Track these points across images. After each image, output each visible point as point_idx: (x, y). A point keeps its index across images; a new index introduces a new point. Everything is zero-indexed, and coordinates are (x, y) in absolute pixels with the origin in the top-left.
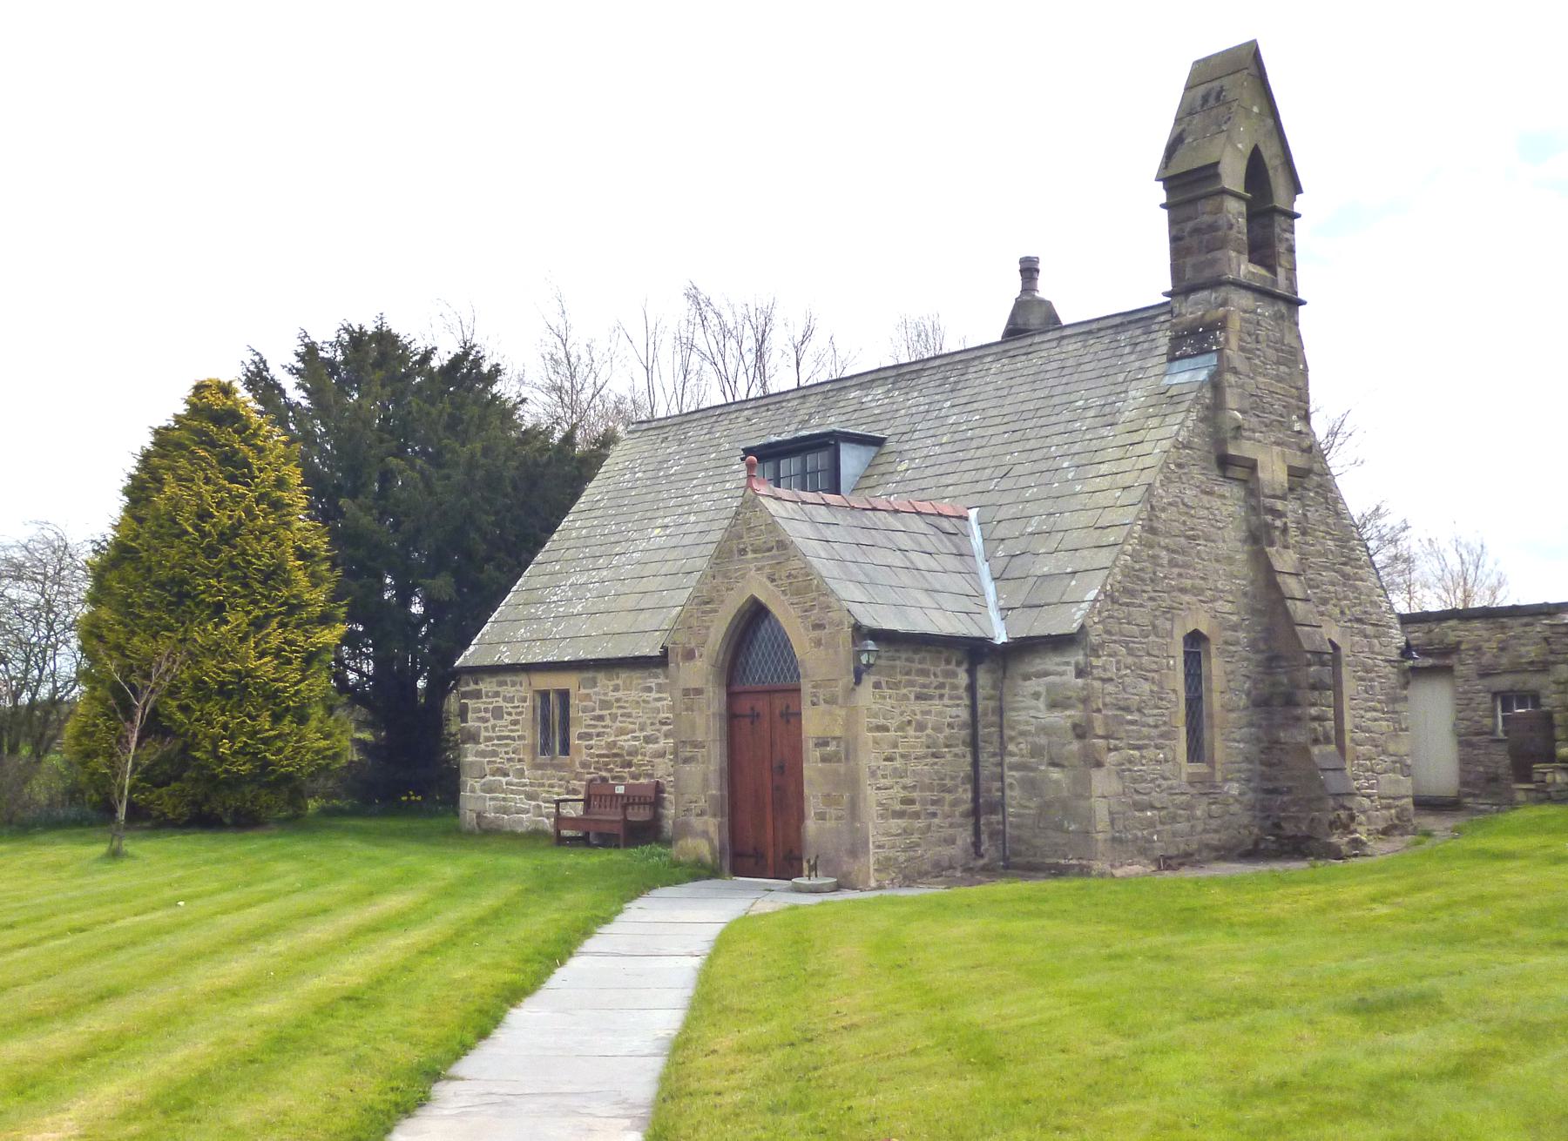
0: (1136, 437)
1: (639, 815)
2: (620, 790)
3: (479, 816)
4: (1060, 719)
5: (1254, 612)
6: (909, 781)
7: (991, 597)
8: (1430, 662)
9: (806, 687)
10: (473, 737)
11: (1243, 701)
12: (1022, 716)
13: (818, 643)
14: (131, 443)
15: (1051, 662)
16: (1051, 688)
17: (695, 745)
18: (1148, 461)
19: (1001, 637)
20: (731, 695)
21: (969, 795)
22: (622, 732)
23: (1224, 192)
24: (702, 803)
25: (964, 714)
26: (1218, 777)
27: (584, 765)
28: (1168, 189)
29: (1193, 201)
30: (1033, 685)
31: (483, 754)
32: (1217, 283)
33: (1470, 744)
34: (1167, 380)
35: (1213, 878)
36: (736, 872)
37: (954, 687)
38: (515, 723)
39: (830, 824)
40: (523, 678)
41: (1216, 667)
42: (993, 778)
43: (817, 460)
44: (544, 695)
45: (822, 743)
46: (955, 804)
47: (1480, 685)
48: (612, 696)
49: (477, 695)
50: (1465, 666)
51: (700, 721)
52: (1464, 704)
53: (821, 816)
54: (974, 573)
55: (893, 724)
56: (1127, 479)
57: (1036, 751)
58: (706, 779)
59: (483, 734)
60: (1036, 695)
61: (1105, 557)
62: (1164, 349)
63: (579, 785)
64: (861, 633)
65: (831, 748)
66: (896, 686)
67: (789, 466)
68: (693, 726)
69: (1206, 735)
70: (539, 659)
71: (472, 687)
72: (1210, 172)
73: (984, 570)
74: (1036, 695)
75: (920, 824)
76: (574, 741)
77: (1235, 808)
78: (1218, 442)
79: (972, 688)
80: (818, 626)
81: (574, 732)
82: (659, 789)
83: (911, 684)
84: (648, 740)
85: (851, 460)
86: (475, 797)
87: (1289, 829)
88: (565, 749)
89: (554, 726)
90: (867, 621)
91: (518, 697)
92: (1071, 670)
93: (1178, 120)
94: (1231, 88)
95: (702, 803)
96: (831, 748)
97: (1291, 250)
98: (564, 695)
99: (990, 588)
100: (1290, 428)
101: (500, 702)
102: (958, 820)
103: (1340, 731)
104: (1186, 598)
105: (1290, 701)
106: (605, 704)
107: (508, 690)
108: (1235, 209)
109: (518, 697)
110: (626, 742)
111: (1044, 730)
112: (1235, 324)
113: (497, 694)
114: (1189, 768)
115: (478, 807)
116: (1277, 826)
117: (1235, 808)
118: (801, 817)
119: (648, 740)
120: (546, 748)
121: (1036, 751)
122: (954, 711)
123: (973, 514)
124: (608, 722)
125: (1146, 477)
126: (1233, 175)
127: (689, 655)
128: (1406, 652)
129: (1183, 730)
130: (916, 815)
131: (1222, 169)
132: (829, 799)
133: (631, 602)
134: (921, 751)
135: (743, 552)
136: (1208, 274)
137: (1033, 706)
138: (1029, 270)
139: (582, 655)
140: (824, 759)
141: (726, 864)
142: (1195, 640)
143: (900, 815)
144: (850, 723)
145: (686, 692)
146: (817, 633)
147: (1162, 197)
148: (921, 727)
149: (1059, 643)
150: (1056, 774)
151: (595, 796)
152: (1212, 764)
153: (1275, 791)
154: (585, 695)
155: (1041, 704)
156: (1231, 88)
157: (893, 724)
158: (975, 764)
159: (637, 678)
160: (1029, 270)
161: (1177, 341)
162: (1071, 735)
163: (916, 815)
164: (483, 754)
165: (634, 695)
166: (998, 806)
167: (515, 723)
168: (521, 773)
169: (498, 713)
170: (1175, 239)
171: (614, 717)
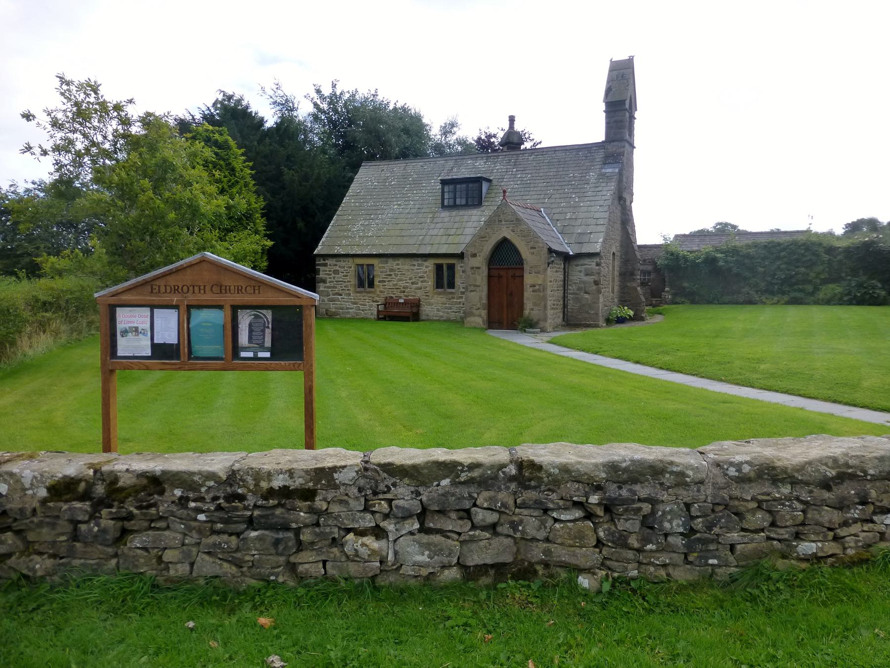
2: (401, 301)
9: (526, 267)
10: (324, 281)
12: (575, 278)
13: (533, 253)
14: (860, 218)
16: (586, 270)
17: (475, 286)
18: (606, 198)
20: (489, 269)
22: (401, 280)
27: (381, 292)
28: (607, 106)
29: (616, 111)
30: (579, 268)
34: (603, 171)
39: (534, 312)
40: (351, 260)
44: (362, 265)
48: (396, 267)
49: (325, 265)
51: (479, 278)
56: (601, 203)
57: (579, 289)
58: (481, 298)
59: (328, 280)
64: (550, 251)
65: (537, 287)
71: (322, 262)
74: (580, 271)
76: (376, 283)
79: (564, 269)
80: (532, 248)
84: (413, 283)
90: (555, 247)
91: (350, 266)
92: (594, 264)
93: (608, 82)
95: (478, 306)
96: (537, 287)
101: (337, 268)
106: (392, 270)
107: (342, 264)
113: (336, 265)
115: (327, 307)
119: (413, 283)
121: (579, 289)
124: (393, 276)
127: (474, 255)
132: (535, 304)
137: (578, 274)
138: (512, 120)
140: (533, 291)
144: (544, 280)
145: (472, 268)
146: (532, 250)
150: (587, 296)
154: (380, 269)
155: (582, 274)
159: (408, 261)
160: (512, 120)
161: (607, 157)
162: (593, 284)
165: (406, 267)
170: (608, 123)
171: (396, 275)
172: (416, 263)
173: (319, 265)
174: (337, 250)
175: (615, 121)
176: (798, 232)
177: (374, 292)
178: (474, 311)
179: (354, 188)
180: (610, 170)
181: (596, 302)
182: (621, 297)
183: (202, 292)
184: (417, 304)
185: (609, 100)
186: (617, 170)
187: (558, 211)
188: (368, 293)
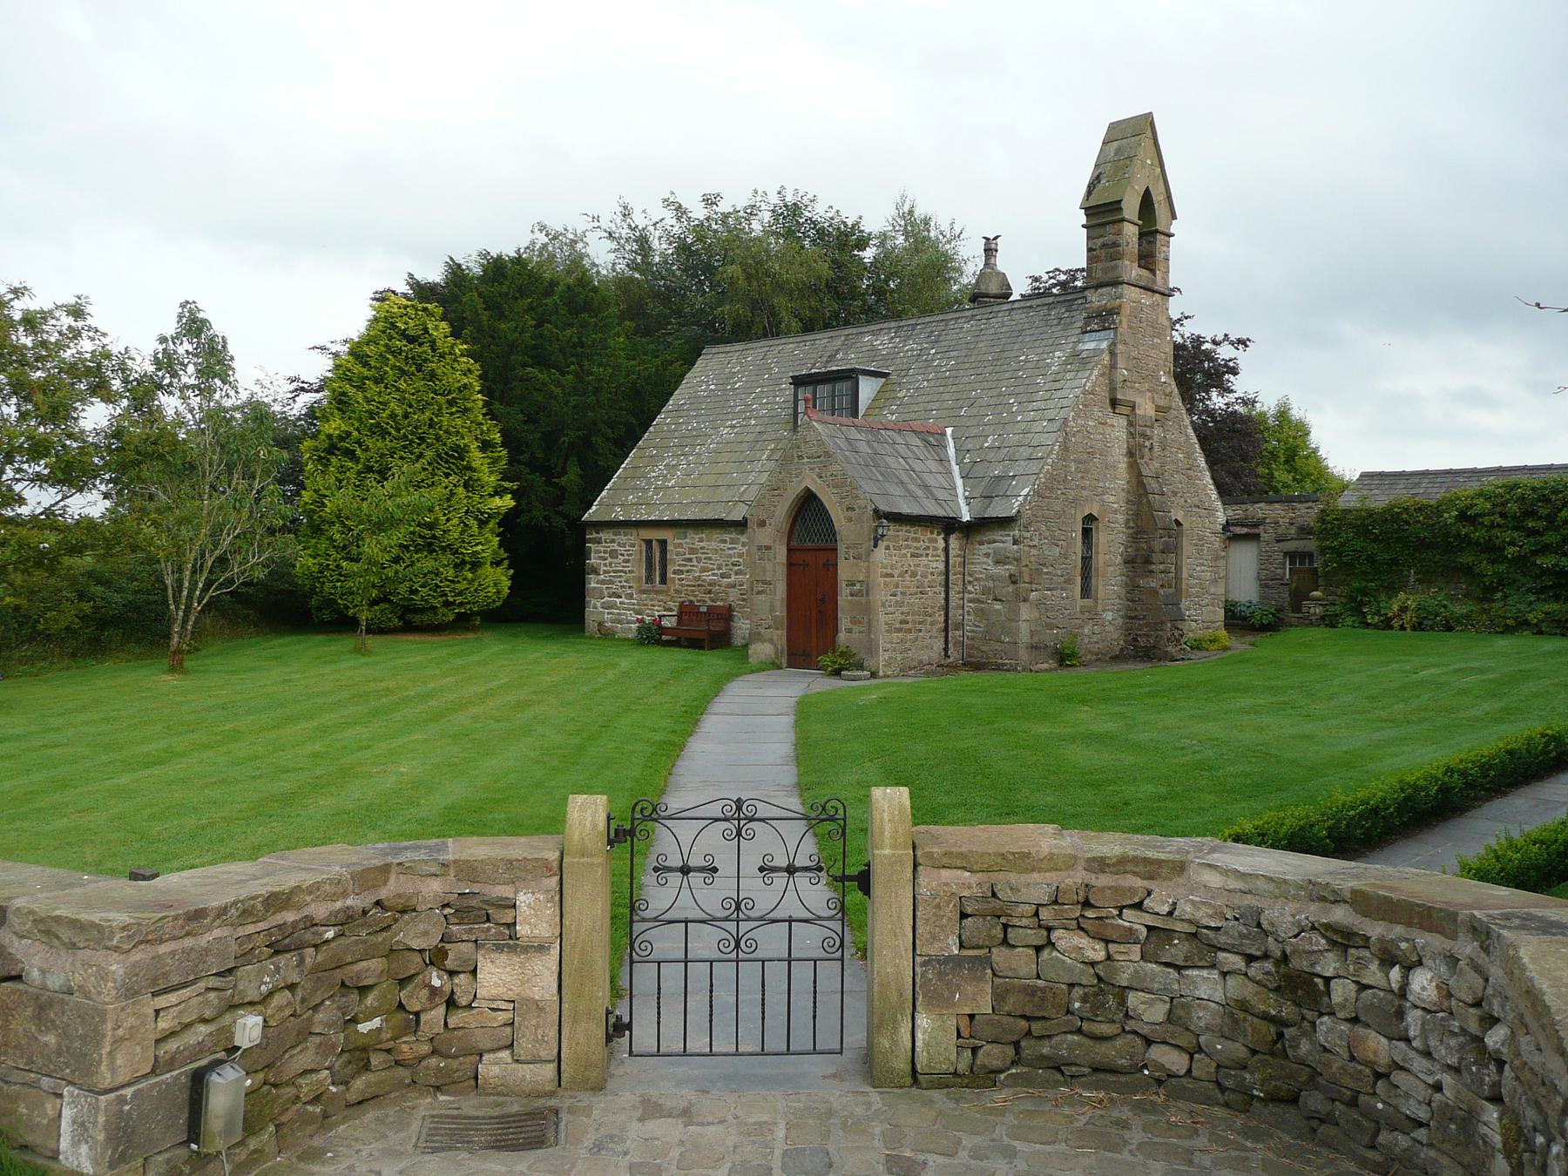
0: (1057, 385)
1: (717, 627)
2: (704, 609)
3: (600, 624)
4: (1000, 570)
5: (1128, 501)
6: (905, 609)
7: (960, 490)
8: (1245, 530)
10: (596, 571)
11: (1119, 560)
13: (850, 520)
15: (998, 535)
18: (1065, 402)
19: (966, 518)
21: (942, 619)
22: (704, 570)
23: (1123, 220)
24: (770, 622)
25: (942, 566)
26: (1100, 608)
27: (677, 591)
30: (985, 548)
31: (603, 582)
32: (1116, 283)
33: (1267, 586)
35: (333, 898)
36: (792, 664)
37: (936, 549)
38: (627, 561)
39: (855, 636)
41: (1101, 538)
42: (958, 607)
43: (843, 386)
44: (649, 543)
45: (851, 584)
46: (932, 624)
47: (1276, 547)
48: (698, 545)
49: (599, 542)
50: (1266, 534)
52: (1264, 560)
53: (849, 631)
54: (949, 473)
55: (896, 573)
56: (1050, 414)
57: (986, 591)
60: (987, 555)
61: (1034, 467)
62: (1080, 324)
63: (674, 605)
64: (878, 514)
65: (858, 587)
66: (899, 548)
67: (823, 390)
68: (764, 570)
69: (1093, 580)
70: (645, 517)
72: (1115, 206)
73: (956, 469)
74: (987, 555)
75: (912, 636)
76: (670, 575)
77: (1111, 629)
78: (1113, 390)
79: (946, 550)
80: (849, 509)
81: (670, 569)
82: (730, 609)
83: (908, 547)
85: (867, 389)
86: (596, 609)
87: (1142, 642)
88: (664, 580)
89: (656, 565)
90: (883, 508)
91: (629, 546)
94: (1132, 141)
95: (770, 622)
96: (858, 587)
97: (1167, 259)
98: (663, 543)
99: (959, 482)
100: (1158, 379)
102: (934, 633)
103: (1178, 578)
104: (1085, 493)
105: (1148, 561)
106: (692, 551)
107: (622, 538)
108: (1130, 231)
109: (629, 546)
110: (708, 577)
111: (992, 578)
112: (1126, 311)
113: (613, 541)
114: (1080, 602)
115: (599, 619)
116: (1135, 640)
117: (1111, 629)
118: (836, 631)
120: (649, 579)
121: (986, 591)
122: (935, 565)
123: (949, 431)
125: (1063, 414)
126: (1131, 208)
127: (762, 524)
128: (1227, 526)
129: (1079, 579)
130: (910, 631)
131: (1123, 205)
133: (711, 479)
134: (913, 590)
135: (800, 457)
136: (1109, 277)
139: (676, 516)
141: (784, 661)
142: (1090, 518)
143: (899, 630)
145: (760, 548)
147: (1084, 220)
148: (914, 575)
149: (1004, 522)
150: (998, 606)
151: (687, 612)
152: (1096, 600)
153: (1135, 618)
156: (1132, 141)
157: (896, 573)
158: (947, 599)
159: (717, 535)
163: (910, 631)
164: (603, 582)
165: (714, 545)
166: (960, 626)
167: (627, 561)
168: (630, 596)
169: (614, 554)
172: (727, 537)
173: (590, 541)
174: (619, 514)
175: (1104, 245)
176: (1550, 468)
177: (665, 592)
178: (763, 631)
179: (678, 398)
180: (1091, 346)
181: (1014, 617)
182: (1129, 609)
183: (768, 588)
184: (725, 615)
185: (1093, 202)
186: (1104, 345)
187: (974, 431)
188: (657, 592)
